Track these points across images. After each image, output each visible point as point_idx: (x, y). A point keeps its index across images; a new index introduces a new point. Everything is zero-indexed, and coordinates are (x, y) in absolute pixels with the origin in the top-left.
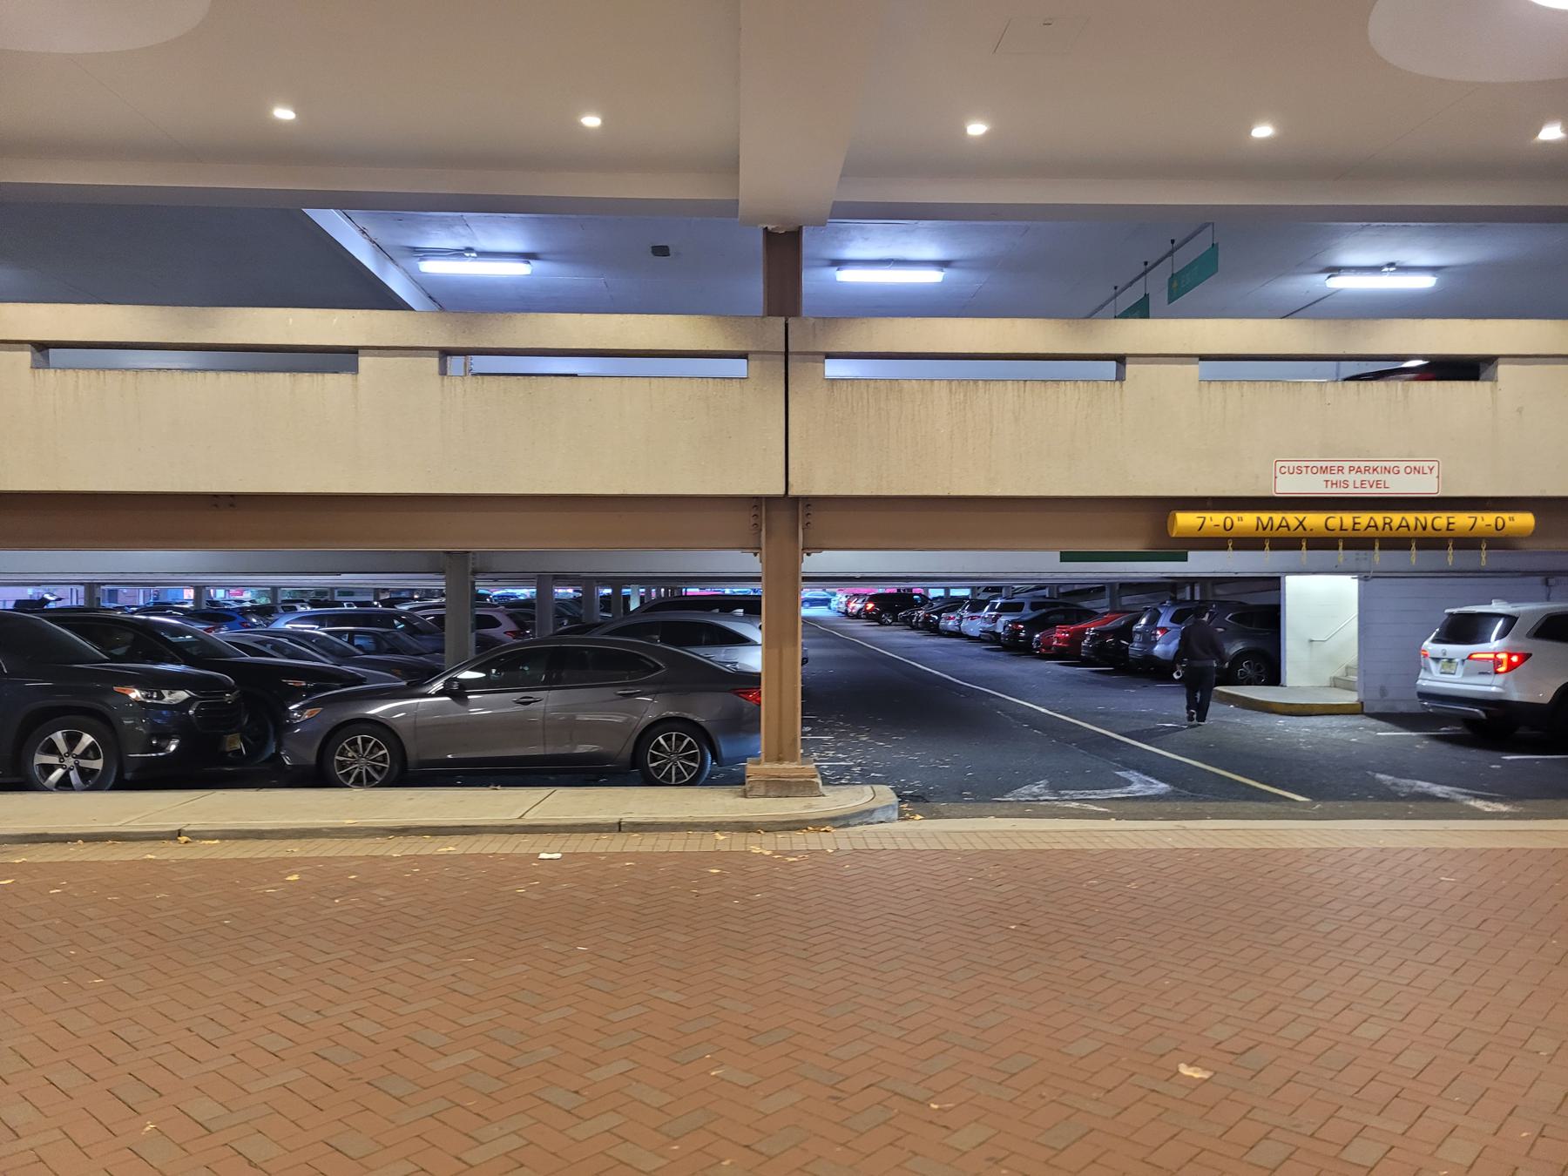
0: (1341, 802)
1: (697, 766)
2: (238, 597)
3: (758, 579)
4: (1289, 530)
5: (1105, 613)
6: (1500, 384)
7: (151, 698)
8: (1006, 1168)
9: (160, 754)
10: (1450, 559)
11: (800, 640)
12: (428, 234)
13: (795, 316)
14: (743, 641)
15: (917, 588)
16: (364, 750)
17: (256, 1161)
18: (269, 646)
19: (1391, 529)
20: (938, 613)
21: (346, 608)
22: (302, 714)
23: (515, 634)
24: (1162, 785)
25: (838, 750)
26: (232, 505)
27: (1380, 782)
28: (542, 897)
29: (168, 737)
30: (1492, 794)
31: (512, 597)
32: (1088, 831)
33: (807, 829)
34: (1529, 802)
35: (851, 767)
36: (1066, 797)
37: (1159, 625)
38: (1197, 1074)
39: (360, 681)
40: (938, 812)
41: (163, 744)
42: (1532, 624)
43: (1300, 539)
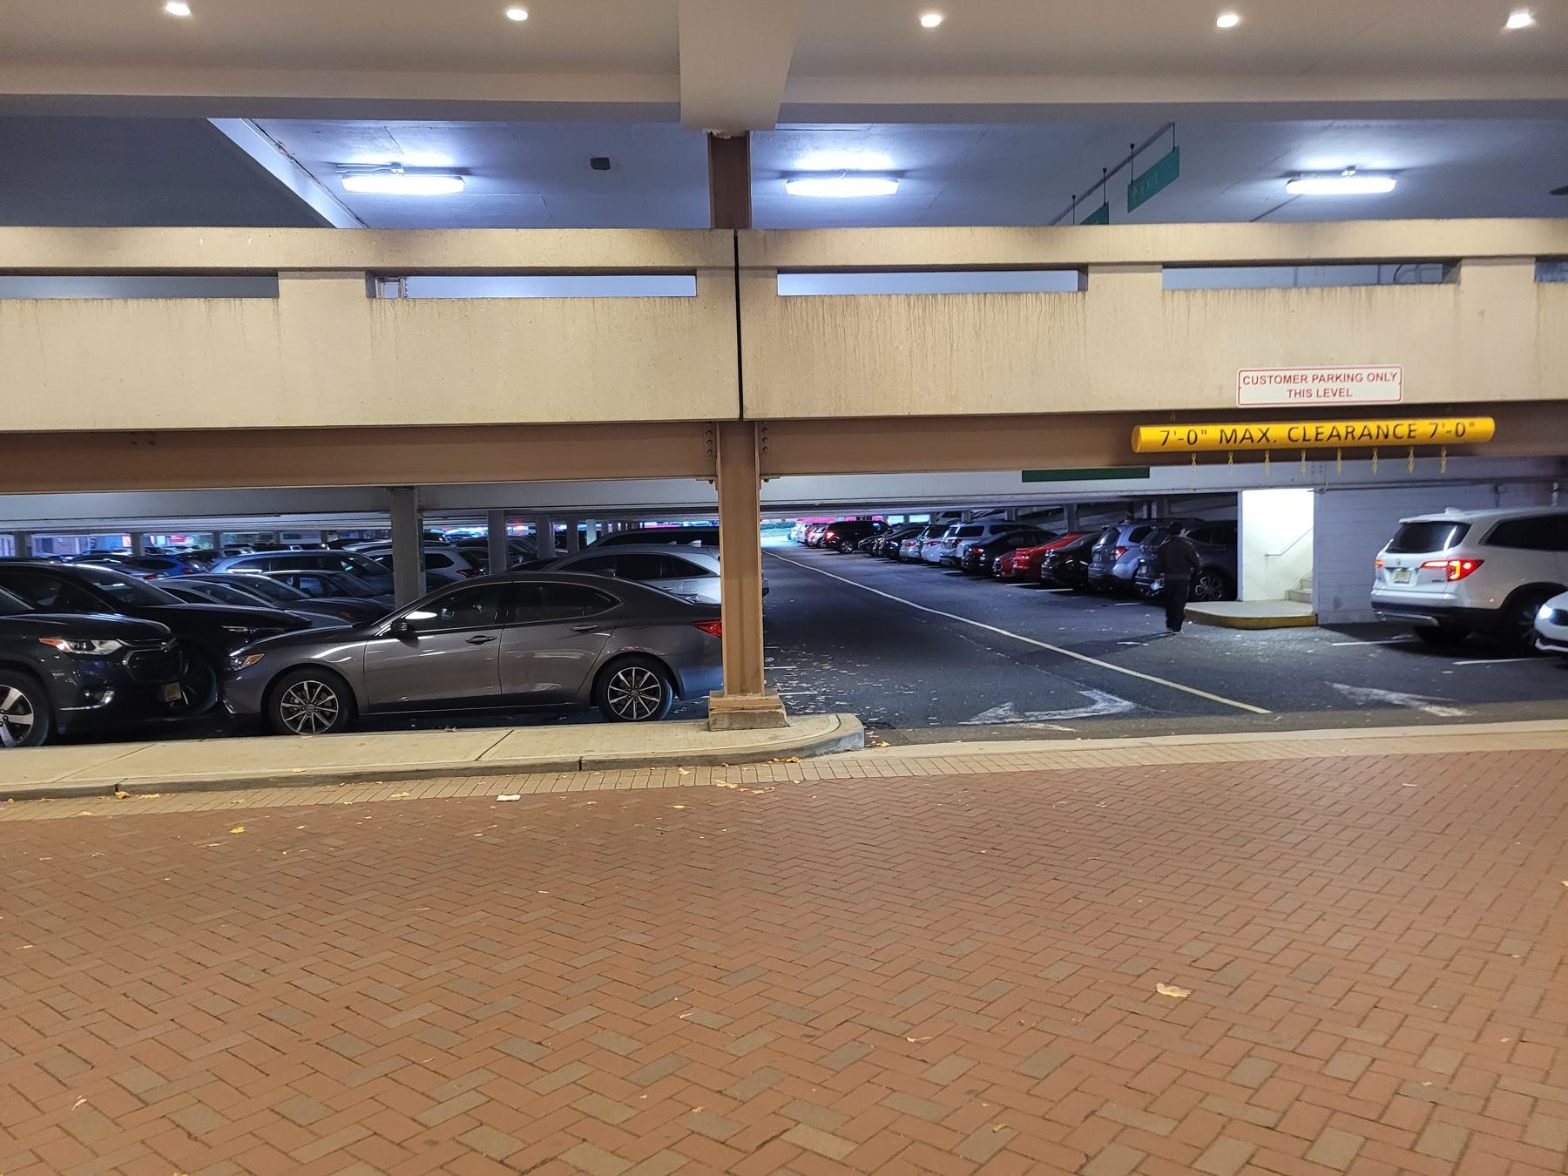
0: (1300, 713)
1: (658, 701)
2: (180, 544)
3: (715, 510)
4: (1252, 441)
5: (1065, 535)
6: (1463, 287)
7: (81, 649)
8: (988, 1101)
9: (95, 707)
10: (1411, 468)
11: (760, 571)
12: (350, 148)
13: (746, 228)
14: (702, 572)
15: (877, 515)
16: (311, 696)
17: (195, 1133)
18: (209, 591)
19: (1353, 438)
20: (899, 540)
21: (292, 551)
22: (243, 661)
23: (469, 573)
24: (1126, 703)
25: (801, 679)
26: (152, 443)
27: (1338, 691)
28: (501, 840)
29: (103, 690)
30: (1443, 699)
31: (465, 536)
32: (1055, 751)
33: (773, 761)
34: (1483, 706)
35: (815, 696)
36: (1032, 719)
37: (1118, 545)
38: (1176, 993)
39: (306, 625)
40: (905, 738)
41: (96, 696)
42: (1485, 530)
43: (1264, 451)
